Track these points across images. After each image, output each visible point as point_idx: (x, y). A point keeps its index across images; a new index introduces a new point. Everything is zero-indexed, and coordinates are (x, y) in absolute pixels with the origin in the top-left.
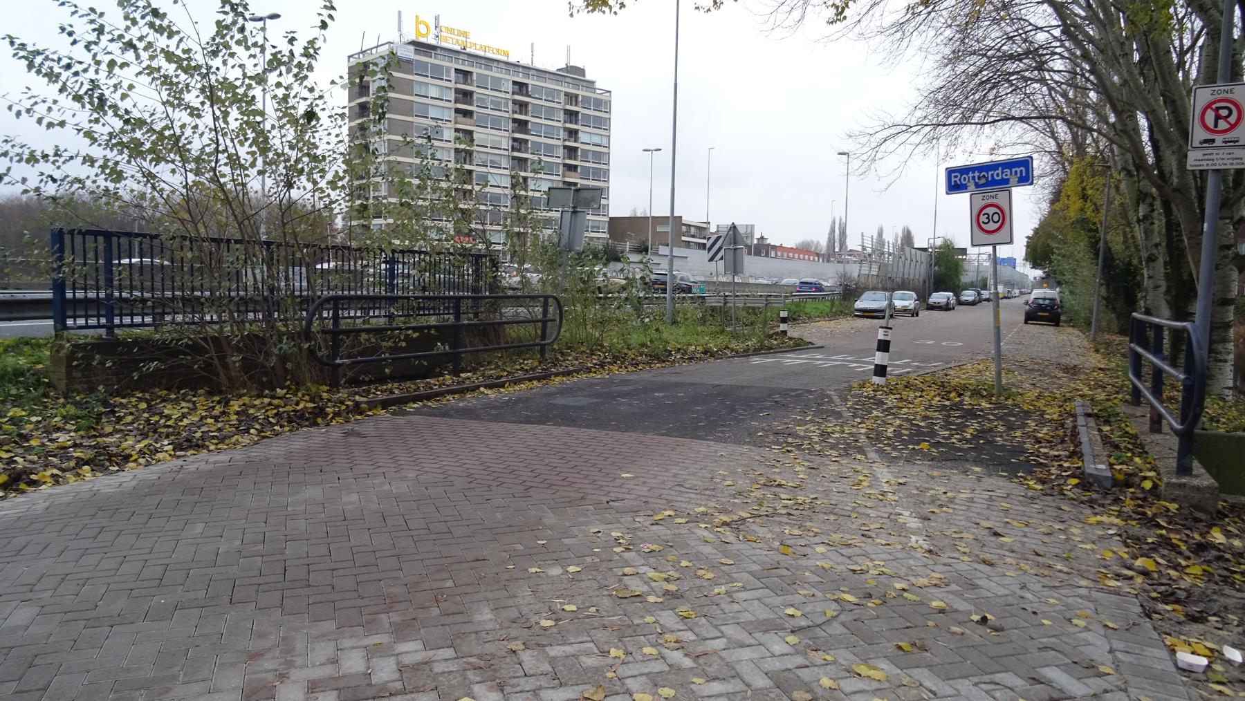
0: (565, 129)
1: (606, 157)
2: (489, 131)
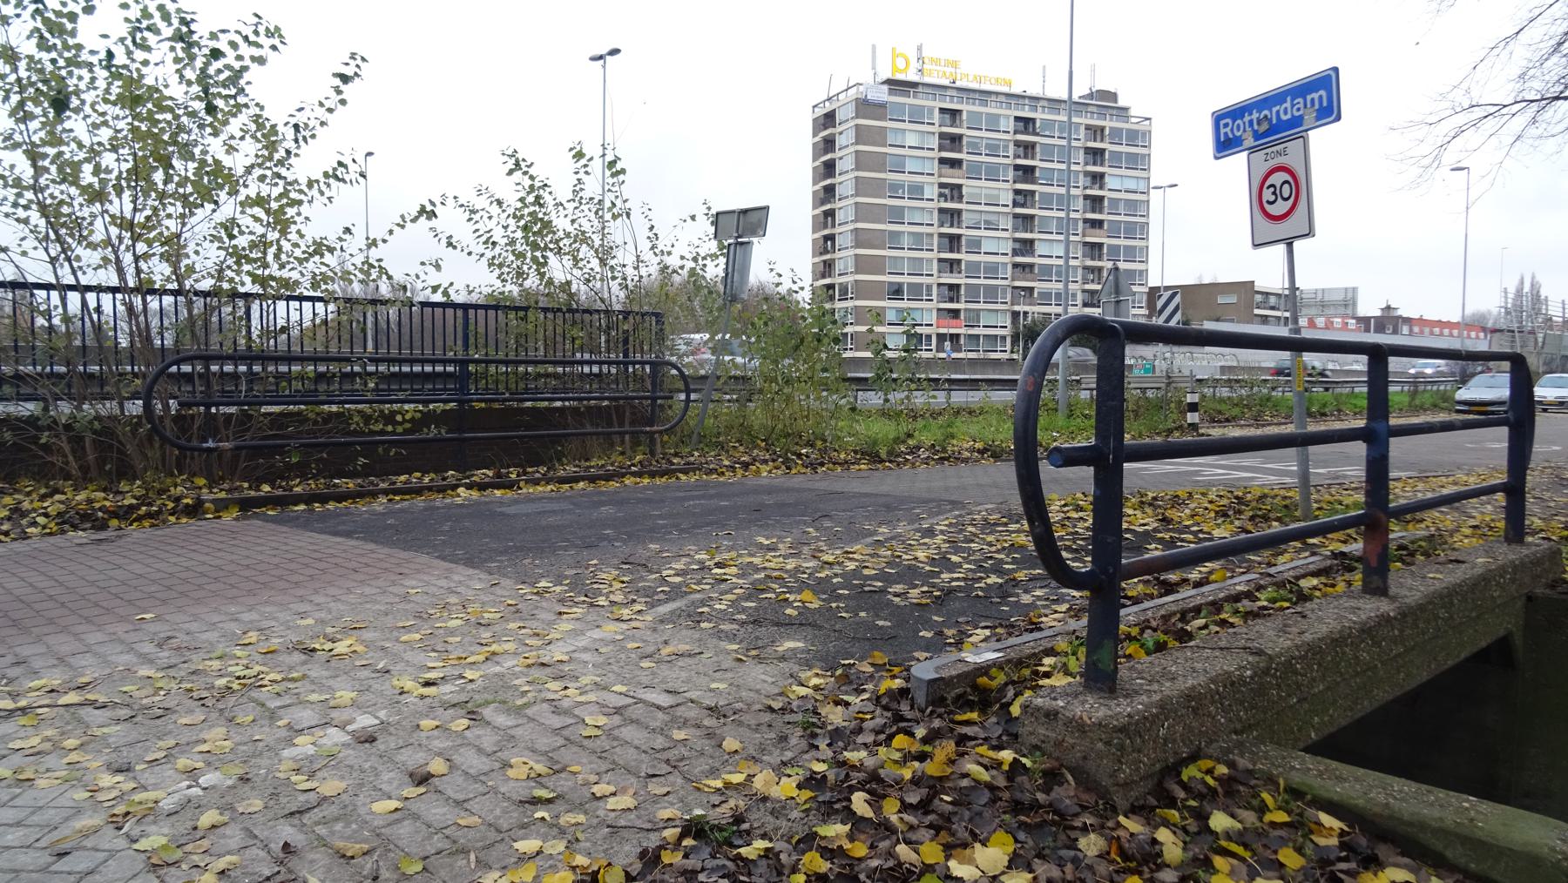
0: (1086, 174)
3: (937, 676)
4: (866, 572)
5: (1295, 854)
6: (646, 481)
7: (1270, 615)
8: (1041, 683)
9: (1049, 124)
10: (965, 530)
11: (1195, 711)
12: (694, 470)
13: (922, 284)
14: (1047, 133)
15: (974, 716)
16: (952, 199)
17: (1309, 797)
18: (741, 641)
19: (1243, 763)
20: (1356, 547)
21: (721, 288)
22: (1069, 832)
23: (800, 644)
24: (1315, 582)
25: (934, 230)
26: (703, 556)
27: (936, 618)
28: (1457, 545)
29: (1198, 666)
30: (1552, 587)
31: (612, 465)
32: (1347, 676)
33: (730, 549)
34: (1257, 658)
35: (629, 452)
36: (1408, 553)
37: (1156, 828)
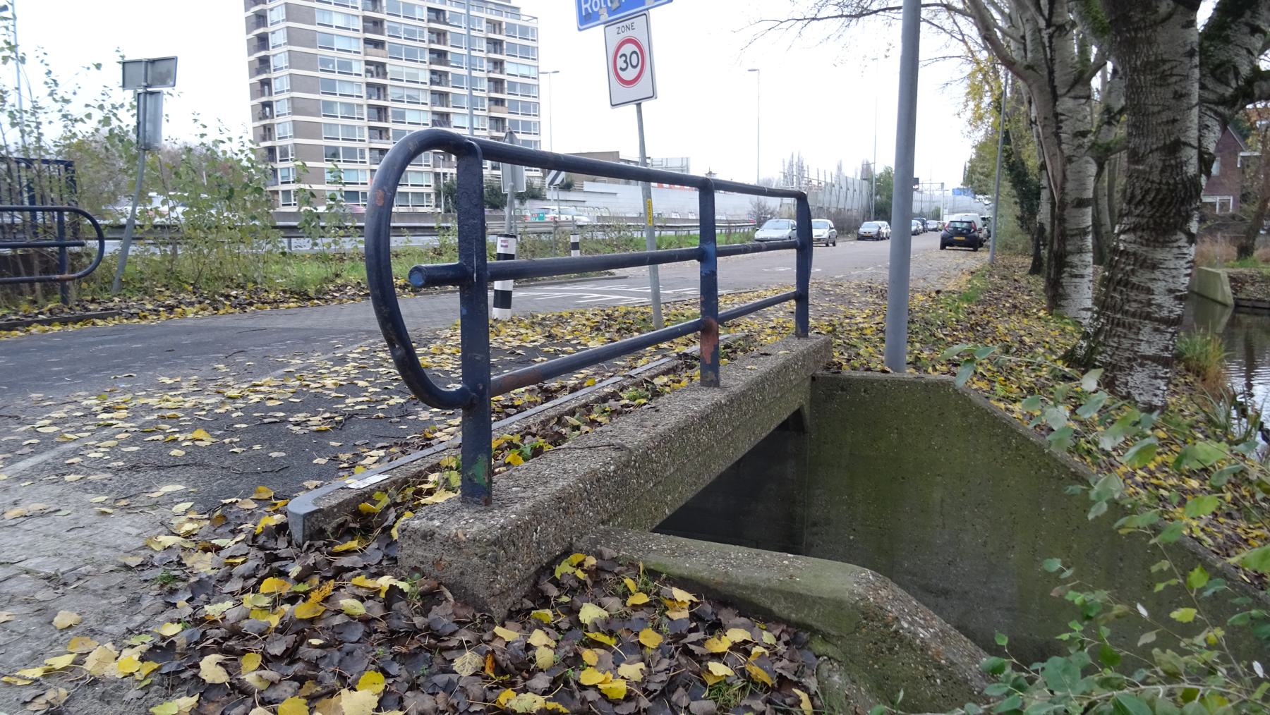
0: (489, 60)
1: (535, 90)
2: (403, 63)
3: (316, 508)
4: (270, 403)
5: (654, 633)
6: (57, 328)
7: (631, 412)
8: (423, 501)
9: (456, 16)
10: (376, 357)
11: (565, 511)
12: (113, 315)
13: (355, 149)
14: (456, 24)
15: (353, 544)
16: (378, 75)
17: (664, 576)
18: (111, 491)
19: (608, 552)
20: (695, 349)
21: (133, 137)
22: (444, 654)
23: (180, 487)
24: (665, 379)
25: (364, 101)
26: (92, 401)
27: (333, 443)
28: (763, 342)
29: (569, 467)
30: (827, 369)
31: (16, 314)
32: (691, 458)
33: (125, 391)
34: (619, 454)
35: (41, 301)
36: (731, 349)
37: (531, 631)
